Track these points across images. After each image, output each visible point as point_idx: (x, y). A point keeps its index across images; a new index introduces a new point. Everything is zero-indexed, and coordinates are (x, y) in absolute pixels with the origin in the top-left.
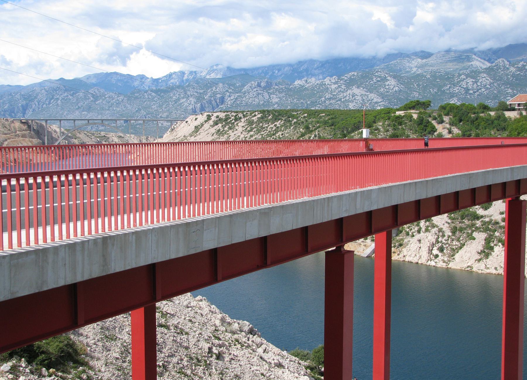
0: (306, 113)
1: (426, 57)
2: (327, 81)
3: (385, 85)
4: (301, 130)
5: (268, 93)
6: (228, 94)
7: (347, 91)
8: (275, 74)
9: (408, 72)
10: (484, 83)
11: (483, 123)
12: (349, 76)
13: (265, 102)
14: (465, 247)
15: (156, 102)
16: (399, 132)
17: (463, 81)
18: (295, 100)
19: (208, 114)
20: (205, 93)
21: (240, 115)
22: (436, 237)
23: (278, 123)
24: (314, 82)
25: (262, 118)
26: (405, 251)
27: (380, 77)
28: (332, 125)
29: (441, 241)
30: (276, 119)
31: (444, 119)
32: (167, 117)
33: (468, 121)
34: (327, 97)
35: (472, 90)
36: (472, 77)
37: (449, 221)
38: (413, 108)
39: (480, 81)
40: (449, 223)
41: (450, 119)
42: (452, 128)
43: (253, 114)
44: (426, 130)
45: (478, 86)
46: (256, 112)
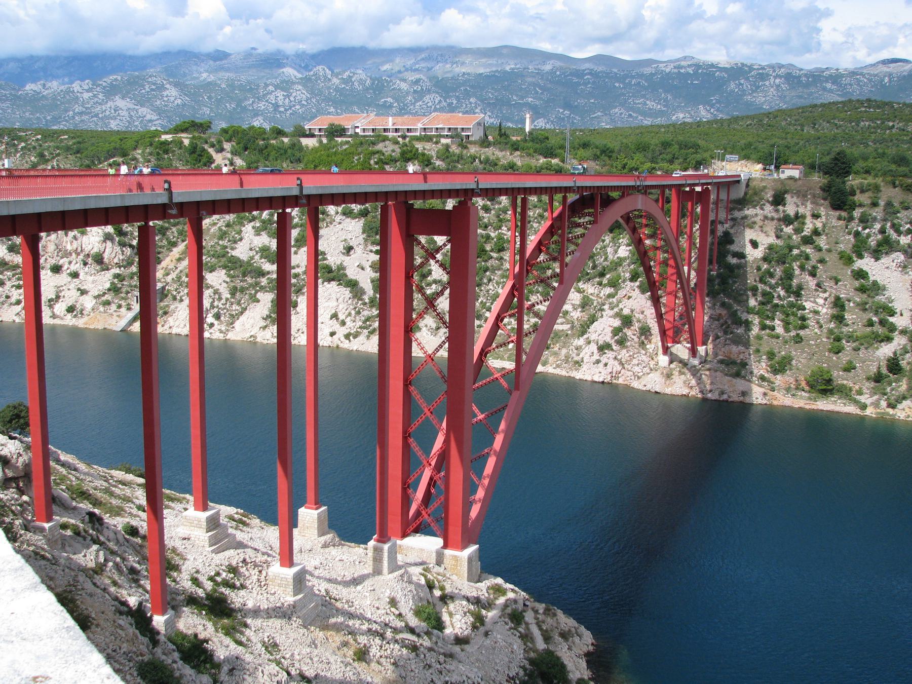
0: (40, 134)
1: (221, 60)
4: (33, 158)
7: (107, 102)
10: (299, 98)
11: (274, 152)
12: (109, 82)
14: (247, 311)
16: (164, 163)
17: (271, 94)
22: (211, 300)
24: (56, 88)
26: (171, 320)
27: (154, 84)
28: (78, 152)
29: (218, 306)
31: (225, 147)
33: (255, 150)
34: (77, 110)
35: (284, 107)
36: (283, 89)
37: (228, 280)
38: (185, 130)
39: (294, 94)
40: (227, 283)
41: (233, 146)
42: (235, 158)
44: (200, 161)
45: (291, 102)
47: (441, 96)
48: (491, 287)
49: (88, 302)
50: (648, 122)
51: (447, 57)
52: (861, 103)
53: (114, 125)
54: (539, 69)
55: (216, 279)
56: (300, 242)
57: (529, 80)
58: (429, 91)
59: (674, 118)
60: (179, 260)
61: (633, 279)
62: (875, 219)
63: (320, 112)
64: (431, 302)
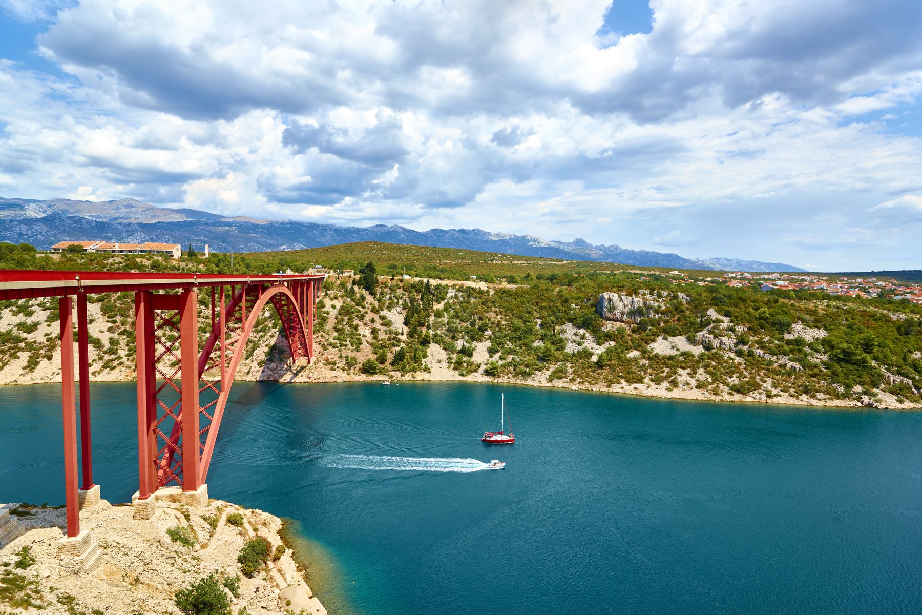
45: (33, 232)
47: (146, 234)
62: (387, 293)
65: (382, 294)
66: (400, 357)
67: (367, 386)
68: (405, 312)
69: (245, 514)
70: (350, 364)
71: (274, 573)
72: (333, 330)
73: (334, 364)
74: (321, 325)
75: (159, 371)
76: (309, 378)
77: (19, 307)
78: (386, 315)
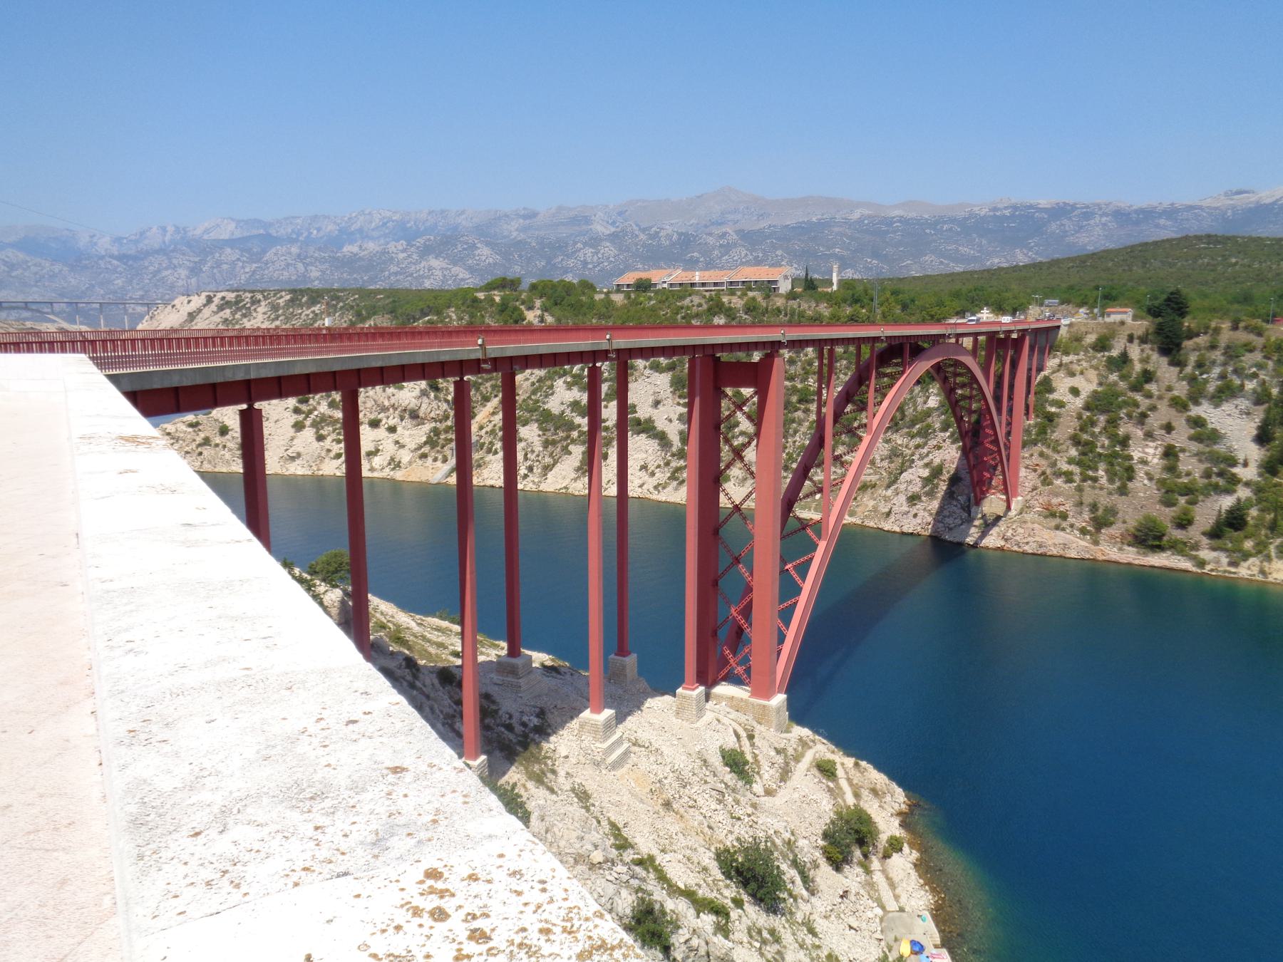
2: (392, 247)
3: (474, 255)
5: (304, 263)
6: (241, 264)
8: (313, 236)
9: (505, 237)
12: (422, 242)
13: (299, 277)
15: (121, 274)
18: (345, 275)
19: (207, 294)
20: (203, 262)
21: (259, 296)
23: (317, 308)
25: (292, 300)
26: (485, 473)
27: (467, 243)
30: (313, 302)
32: (142, 297)
36: (592, 246)
37: (541, 433)
42: (546, 314)
43: (278, 296)
46: (282, 291)
48: (798, 439)
49: (405, 456)
50: (959, 268)
51: (753, 210)
52: (1198, 238)
53: (427, 284)
54: (846, 219)
55: (529, 433)
56: (609, 398)
57: (836, 229)
58: (735, 245)
59: (988, 263)
60: (493, 414)
61: (944, 429)
63: (628, 268)
64: (738, 453)
65: (1200, 365)
66: (1234, 521)
67: (1144, 581)
68: (1259, 414)
69: (843, 764)
70: (1101, 522)
71: (878, 877)
72: (1069, 442)
73: (1064, 516)
74: (1042, 431)
75: (727, 494)
76: (1006, 540)
77: (574, 376)
78: (1203, 415)
